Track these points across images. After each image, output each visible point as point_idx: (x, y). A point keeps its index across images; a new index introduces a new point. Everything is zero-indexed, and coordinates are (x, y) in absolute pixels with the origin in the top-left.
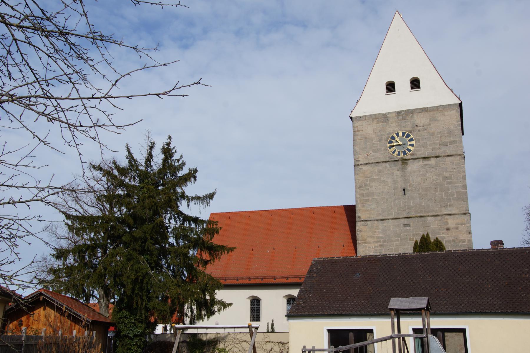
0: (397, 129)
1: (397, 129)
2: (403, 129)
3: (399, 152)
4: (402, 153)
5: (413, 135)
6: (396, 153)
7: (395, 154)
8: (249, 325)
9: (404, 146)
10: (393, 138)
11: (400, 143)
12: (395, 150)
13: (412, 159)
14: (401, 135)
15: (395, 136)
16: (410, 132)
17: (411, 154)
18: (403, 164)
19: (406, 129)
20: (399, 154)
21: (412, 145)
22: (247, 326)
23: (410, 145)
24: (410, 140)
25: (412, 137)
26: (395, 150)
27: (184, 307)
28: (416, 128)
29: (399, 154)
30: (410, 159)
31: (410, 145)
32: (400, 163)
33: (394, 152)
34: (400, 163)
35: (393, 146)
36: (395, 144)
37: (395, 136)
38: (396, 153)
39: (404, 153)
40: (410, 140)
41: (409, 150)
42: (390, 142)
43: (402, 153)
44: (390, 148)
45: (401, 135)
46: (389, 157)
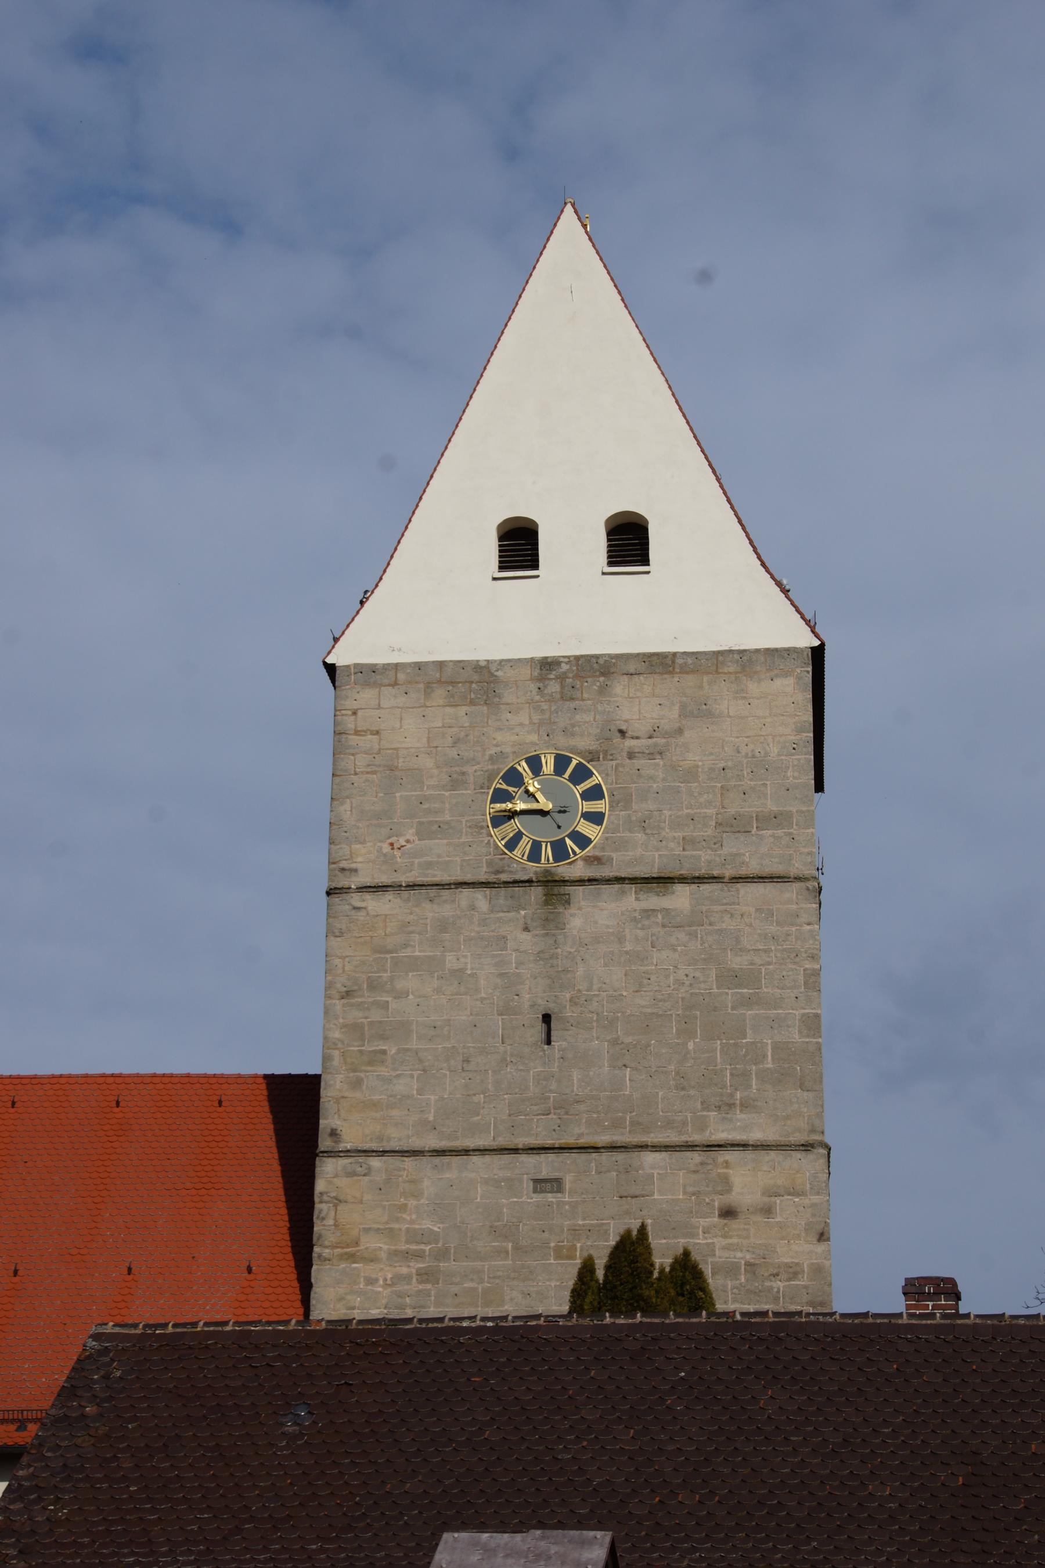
0: (534, 738)
1: (534, 738)
3: (536, 847)
4: (547, 852)
5: (605, 775)
6: (524, 846)
7: (517, 852)
12: (519, 836)
13: (592, 881)
14: (548, 765)
15: (524, 768)
16: (593, 757)
18: (549, 899)
19: (572, 742)
20: (535, 855)
21: (596, 818)
24: (587, 796)
26: (519, 836)
28: (617, 740)
29: (535, 855)
30: (581, 882)
32: (536, 893)
33: (512, 844)
35: (513, 814)
36: (520, 806)
37: (524, 768)
38: (524, 846)
39: (560, 852)
41: (582, 841)
42: (501, 796)
43: (547, 852)
44: (498, 820)
45: (548, 765)
46: (489, 864)
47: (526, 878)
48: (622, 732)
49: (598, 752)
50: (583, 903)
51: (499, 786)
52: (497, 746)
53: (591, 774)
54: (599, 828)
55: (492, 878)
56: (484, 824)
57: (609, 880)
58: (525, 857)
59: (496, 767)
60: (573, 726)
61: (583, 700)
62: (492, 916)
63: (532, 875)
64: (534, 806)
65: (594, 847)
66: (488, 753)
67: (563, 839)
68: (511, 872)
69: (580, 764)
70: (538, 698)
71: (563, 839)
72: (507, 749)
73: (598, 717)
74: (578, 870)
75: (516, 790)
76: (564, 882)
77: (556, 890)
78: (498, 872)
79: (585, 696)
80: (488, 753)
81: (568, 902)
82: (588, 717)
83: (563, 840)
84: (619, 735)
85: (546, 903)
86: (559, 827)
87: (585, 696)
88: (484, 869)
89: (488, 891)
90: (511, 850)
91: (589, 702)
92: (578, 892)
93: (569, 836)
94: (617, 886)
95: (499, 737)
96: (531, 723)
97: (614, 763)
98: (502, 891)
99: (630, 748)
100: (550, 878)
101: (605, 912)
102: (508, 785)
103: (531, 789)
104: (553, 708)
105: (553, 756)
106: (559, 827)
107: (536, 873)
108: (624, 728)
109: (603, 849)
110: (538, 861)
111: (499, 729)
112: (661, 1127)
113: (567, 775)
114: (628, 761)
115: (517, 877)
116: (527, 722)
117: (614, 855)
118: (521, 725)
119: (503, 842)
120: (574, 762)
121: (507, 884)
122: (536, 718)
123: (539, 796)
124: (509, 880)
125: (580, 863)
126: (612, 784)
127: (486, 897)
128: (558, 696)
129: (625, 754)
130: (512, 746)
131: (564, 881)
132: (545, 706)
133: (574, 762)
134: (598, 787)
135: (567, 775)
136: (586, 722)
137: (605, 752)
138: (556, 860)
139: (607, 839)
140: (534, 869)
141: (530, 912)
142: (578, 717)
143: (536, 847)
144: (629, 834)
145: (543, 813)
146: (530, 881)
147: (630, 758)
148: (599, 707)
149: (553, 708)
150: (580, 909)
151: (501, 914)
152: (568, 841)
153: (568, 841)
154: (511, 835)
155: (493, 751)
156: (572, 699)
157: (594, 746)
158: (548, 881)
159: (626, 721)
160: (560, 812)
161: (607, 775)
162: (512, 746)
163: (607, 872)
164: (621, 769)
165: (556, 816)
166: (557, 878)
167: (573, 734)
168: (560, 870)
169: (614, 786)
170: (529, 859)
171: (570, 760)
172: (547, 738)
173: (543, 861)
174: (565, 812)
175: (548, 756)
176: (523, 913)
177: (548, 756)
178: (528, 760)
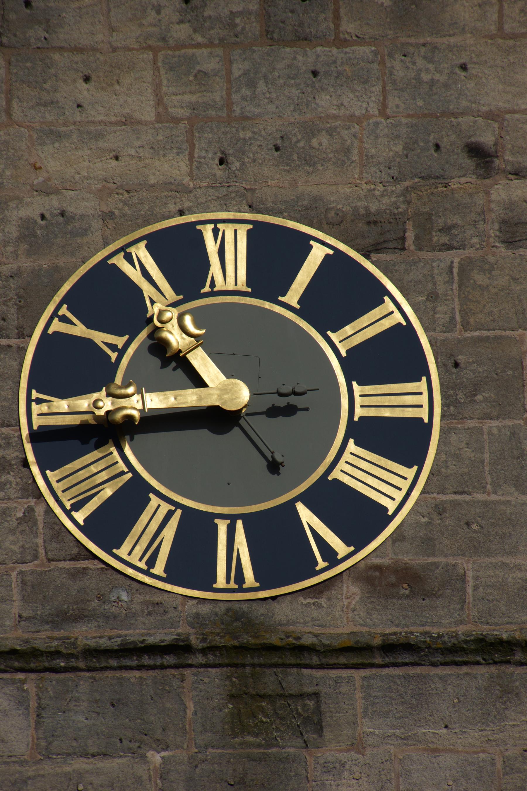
0: (174, 167)
1: (174, 167)
2: (271, 177)
3: (196, 534)
4: (234, 550)
5: (426, 301)
6: (156, 526)
7: (130, 552)
8: (277, 391)
9: (275, 434)
10: (110, 300)
11: (222, 388)
12: (132, 498)
13: (396, 650)
14: (229, 265)
15: (142, 267)
16: (380, 235)
17: (370, 576)
18: (247, 709)
19: (310, 185)
20: (192, 556)
21: (398, 440)
22: (276, 391)
23: (373, 434)
24: (364, 364)
25: (396, 309)
26: (132, 498)
27: (181, 646)
28: (464, 181)
29: (192, 556)
30: (356, 653)
31: (373, 434)
32: (201, 691)
33: (114, 521)
34: (201, 691)
35: (106, 432)
36: (138, 403)
37: (142, 267)
38: (156, 526)
39: (280, 549)
40: (364, 364)
41: (356, 516)
42: (68, 367)
43: (234, 550)
44: (58, 444)
45: (229, 265)
46: (33, 589)
47: (162, 636)
48: (481, 155)
49: (398, 220)
50: (367, 727)
51: (57, 326)
52: (45, 190)
53: (379, 294)
54: (410, 473)
55: (43, 638)
56: (11, 454)
57: (454, 650)
58: (159, 569)
59: (45, 263)
60: (310, 130)
61: (341, 42)
62: (47, 768)
63: (183, 629)
64: (190, 398)
65: (397, 536)
66: (17, 214)
67: (290, 506)
68: (108, 617)
69: (334, 262)
70: (181, 32)
71: (290, 506)
72: (85, 205)
73: (393, 102)
74: (348, 616)
75: (120, 341)
76: (298, 652)
77: (270, 681)
78: (62, 618)
79: (349, 27)
80: (17, 214)
81: (315, 724)
82: (358, 102)
83: (288, 510)
84: (469, 163)
85: (239, 724)
86: (274, 467)
87: (349, 27)
88: (16, 607)
89: (30, 683)
90: (111, 544)
91: (365, 51)
92: (350, 689)
93: (302, 498)
94: (483, 672)
95: (53, 161)
96: (163, 117)
97: (456, 258)
98: (83, 685)
99: (510, 206)
100: (247, 639)
101: (447, 760)
102: (90, 342)
103: (175, 338)
104: (237, 71)
105: (243, 231)
106: (274, 467)
107: (197, 621)
108: (487, 139)
109: (428, 544)
110: (207, 581)
111: (52, 134)
112: (182, 119)
113: (293, 297)
114: (502, 250)
115: (134, 634)
116: (148, 114)
117: (467, 566)
118: (129, 121)
119: (80, 516)
120: (318, 254)
121: (97, 657)
122: (179, 102)
123: (201, 362)
124: (104, 643)
125: (352, 589)
126: (450, 326)
127: (22, 702)
128: (254, 27)
129: (493, 230)
130: (103, 194)
131: (300, 649)
132: (209, 61)
133: (318, 254)
134: (403, 333)
135: (293, 297)
136: (352, 118)
137: (425, 223)
138: (265, 579)
139: (440, 510)
140: (190, 608)
141: (181, 755)
142: (325, 102)
143: (196, 534)
144: (514, 497)
145: (216, 419)
146: (179, 648)
147: (510, 242)
148: (399, 68)
149: (237, 71)
150: (357, 745)
151: (80, 764)
152: (305, 514)
153: (305, 514)
154: (108, 492)
155: (33, 208)
156: (302, 39)
157: (383, 200)
158: (243, 649)
159: (492, 116)
160: (273, 412)
161: (433, 297)
162: (103, 194)
163: (443, 622)
164: (480, 279)
165: (261, 425)
166: (274, 640)
167: (309, 160)
168: (282, 612)
169: (457, 334)
170: (173, 574)
171: (302, 245)
172: (219, 172)
173: (221, 581)
174: (290, 410)
175: (228, 231)
176: (156, 758)
177: (228, 231)
178: (157, 244)
